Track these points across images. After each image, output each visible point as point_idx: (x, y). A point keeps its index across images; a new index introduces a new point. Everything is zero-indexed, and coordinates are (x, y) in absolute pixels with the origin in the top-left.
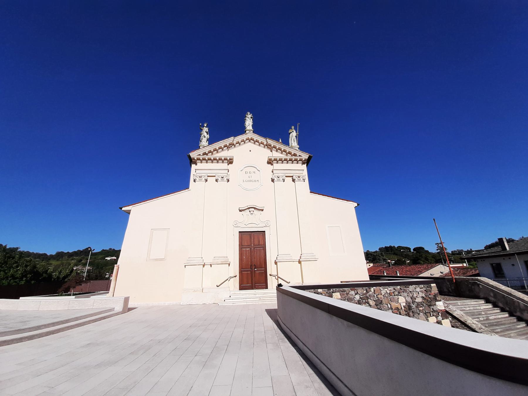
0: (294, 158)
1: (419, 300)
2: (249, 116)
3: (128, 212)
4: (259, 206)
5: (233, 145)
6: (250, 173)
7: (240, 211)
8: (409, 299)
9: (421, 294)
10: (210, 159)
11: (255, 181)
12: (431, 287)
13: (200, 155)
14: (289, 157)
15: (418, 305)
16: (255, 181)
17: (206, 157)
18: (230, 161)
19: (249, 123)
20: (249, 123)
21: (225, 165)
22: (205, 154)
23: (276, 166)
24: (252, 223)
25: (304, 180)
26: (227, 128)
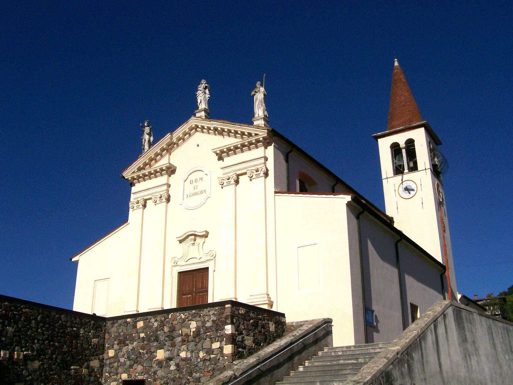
0: (253, 139)
1: (208, 324)
2: (203, 84)
3: (77, 262)
4: (200, 230)
5: (175, 144)
6: (196, 181)
7: (181, 242)
8: (200, 324)
9: (213, 318)
10: (156, 172)
11: (201, 193)
12: (225, 308)
13: (134, 172)
14: (246, 140)
15: (207, 329)
16: (201, 193)
17: (146, 172)
18: (171, 170)
19: (202, 97)
20: (202, 97)
21: (163, 179)
22: (140, 169)
23: (229, 160)
24: (192, 258)
25: (266, 174)
26: (171, 117)
